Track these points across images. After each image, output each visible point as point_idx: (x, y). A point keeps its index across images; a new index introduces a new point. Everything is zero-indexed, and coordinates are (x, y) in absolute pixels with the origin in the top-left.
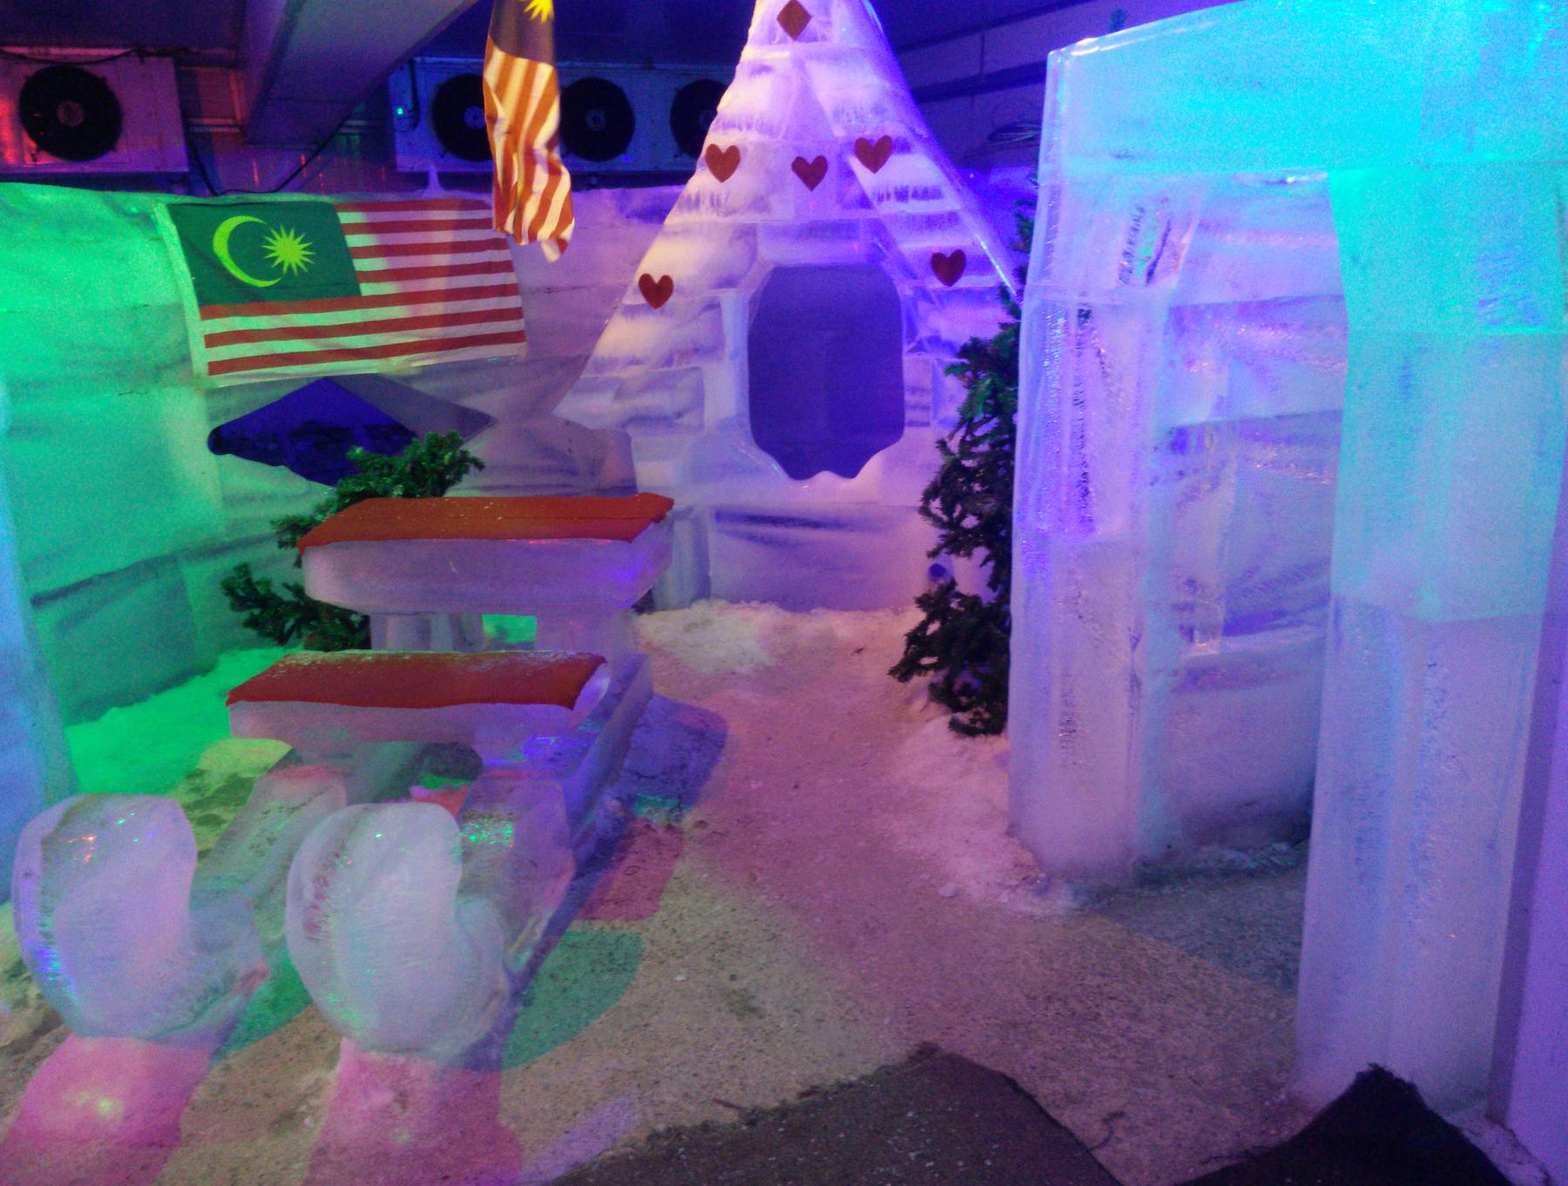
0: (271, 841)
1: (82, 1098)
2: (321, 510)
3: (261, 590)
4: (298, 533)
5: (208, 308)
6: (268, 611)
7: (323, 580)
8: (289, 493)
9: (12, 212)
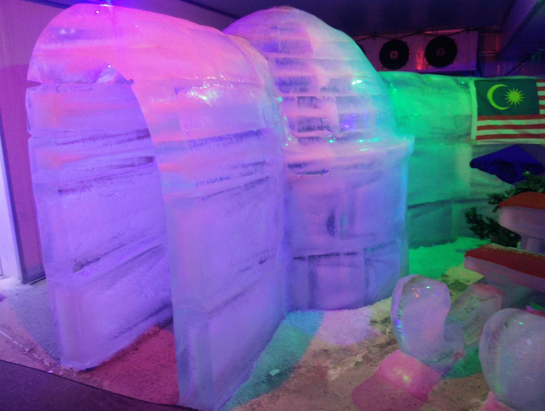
0: (472, 309)
1: (400, 372)
2: (507, 192)
3: (479, 218)
4: (498, 200)
5: (481, 116)
6: (478, 225)
7: (505, 219)
8: (492, 184)
9: (424, 83)
